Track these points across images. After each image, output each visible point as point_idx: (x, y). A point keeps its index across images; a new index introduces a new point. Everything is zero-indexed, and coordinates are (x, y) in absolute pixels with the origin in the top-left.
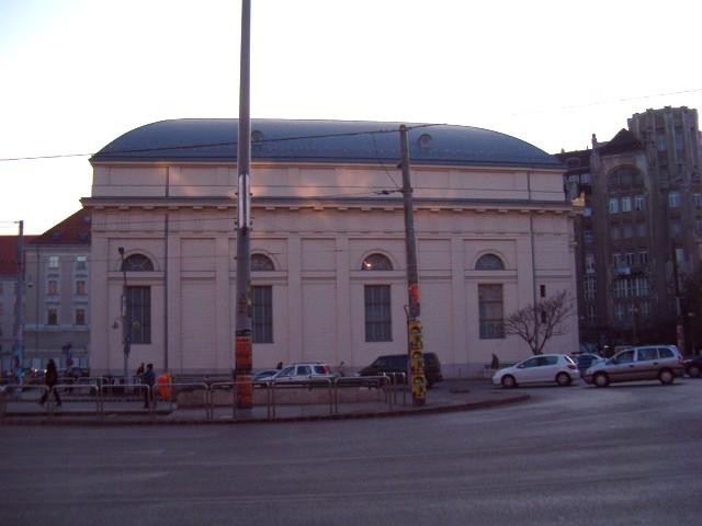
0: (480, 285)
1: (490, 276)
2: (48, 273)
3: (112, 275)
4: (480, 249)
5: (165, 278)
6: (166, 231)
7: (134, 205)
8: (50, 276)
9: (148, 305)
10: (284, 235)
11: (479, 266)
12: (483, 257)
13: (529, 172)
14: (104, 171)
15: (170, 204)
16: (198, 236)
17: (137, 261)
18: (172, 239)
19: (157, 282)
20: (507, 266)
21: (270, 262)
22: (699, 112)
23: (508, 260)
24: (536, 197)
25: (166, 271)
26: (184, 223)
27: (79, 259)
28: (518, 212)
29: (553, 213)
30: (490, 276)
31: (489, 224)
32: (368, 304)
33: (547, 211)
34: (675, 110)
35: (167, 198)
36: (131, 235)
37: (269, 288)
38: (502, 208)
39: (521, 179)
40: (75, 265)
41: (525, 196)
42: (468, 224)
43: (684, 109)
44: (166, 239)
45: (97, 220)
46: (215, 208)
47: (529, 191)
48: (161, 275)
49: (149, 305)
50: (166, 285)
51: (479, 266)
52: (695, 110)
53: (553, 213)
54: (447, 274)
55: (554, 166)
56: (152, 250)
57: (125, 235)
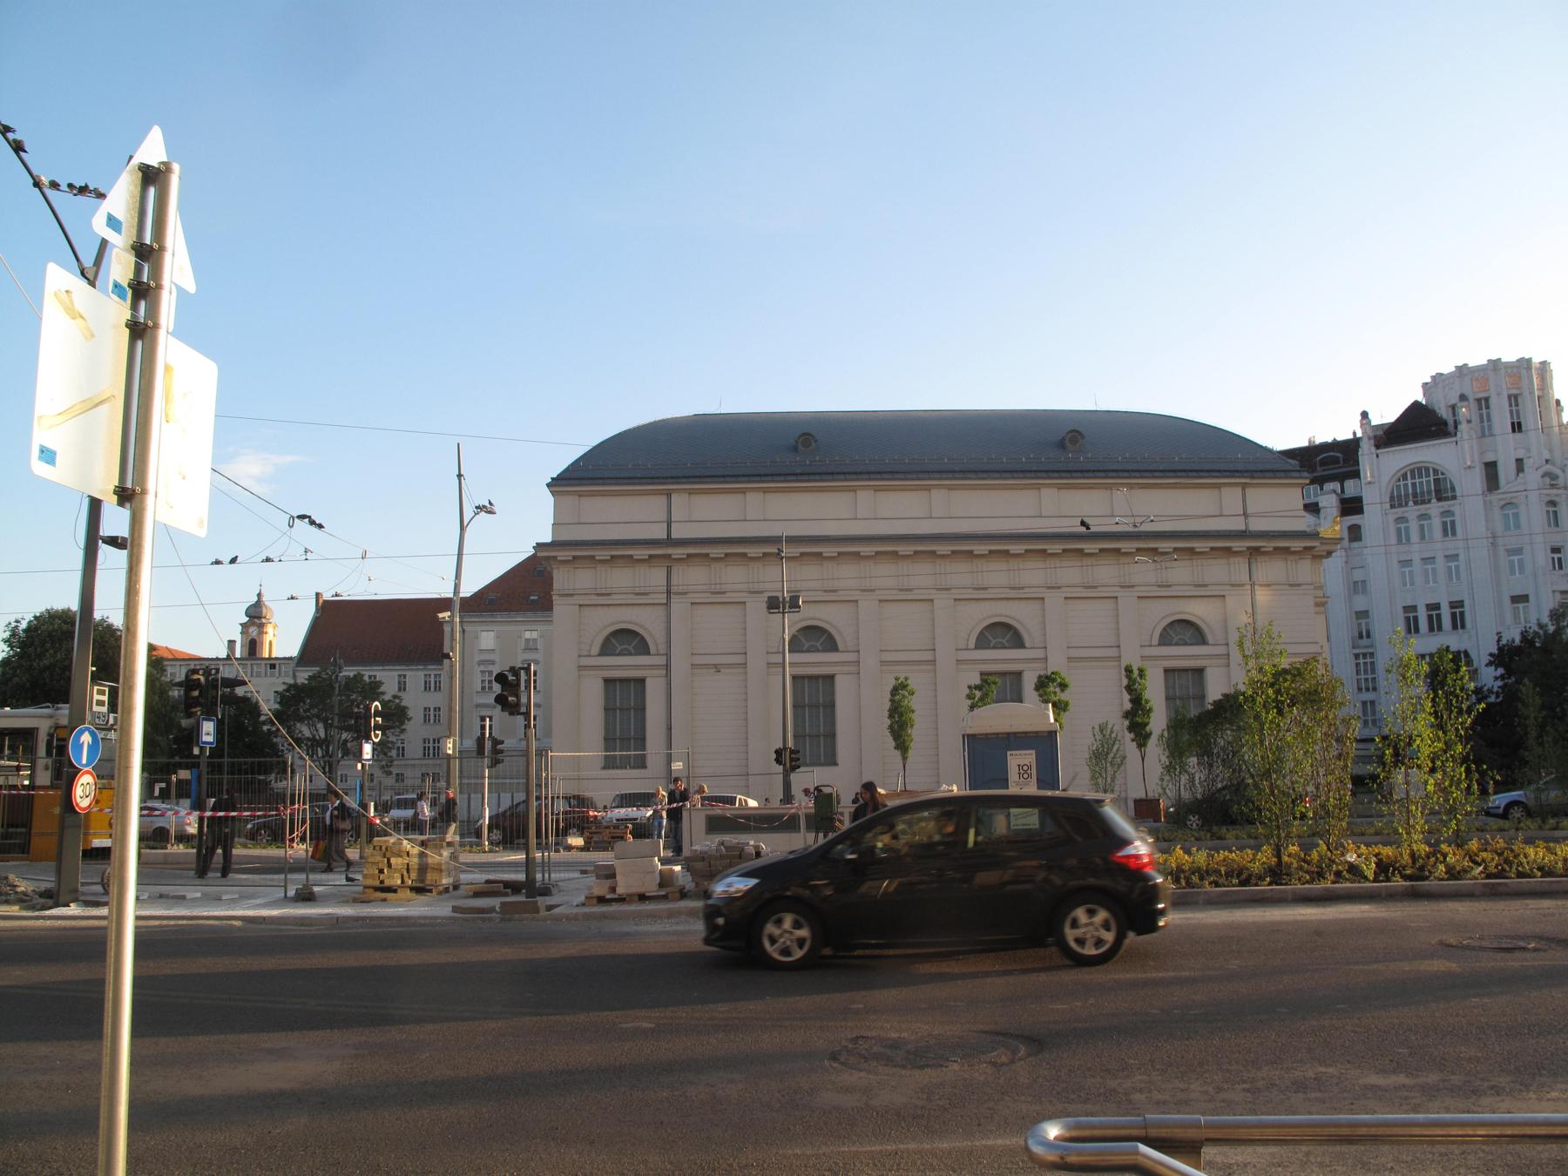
0: (1167, 671)
1: (625, 665)
2: (478, 658)
3: (585, 661)
4: (981, 615)
5: (668, 667)
6: (669, 593)
7: (619, 552)
8: (481, 663)
9: (641, 709)
10: (855, 595)
11: (1165, 640)
12: (1172, 623)
13: (1244, 486)
14: (569, 501)
15: (669, 551)
16: (718, 597)
17: (625, 640)
18: (677, 606)
19: (846, 669)
20: (1210, 638)
21: (830, 637)
22: (1554, 367)
23: (843, 636)
24: (1257, 525)
25: (668, 655)
26: (691, 577)
27: (528, 635)
28: (1228, 551)
29: (1286, 550)
30: (625, 665)
31: (997, 575)
32: (609, 710)
33: (1275, 549)
34: (1509, 365)
35: (670, 542)
36: (615, 599)
37: (830, 678)
38: (1199, 545)
39: (1231, 497)
40: (522, 645)
41: (1237, 525)
42: (960, 575)
43: (1525, 363)
44: (668, 604)
45: (562, 579)
46: (593, 557)
47: (1245, 514)
48: (662, 660)
49: (643, 709)
50: (668, 675)
51: (1165, 640)
52: (127, 326)
53: (1286, 550)
54: (928, 656)
55: (1286, 473)
56: (647, 621)
57: (981, 595)
